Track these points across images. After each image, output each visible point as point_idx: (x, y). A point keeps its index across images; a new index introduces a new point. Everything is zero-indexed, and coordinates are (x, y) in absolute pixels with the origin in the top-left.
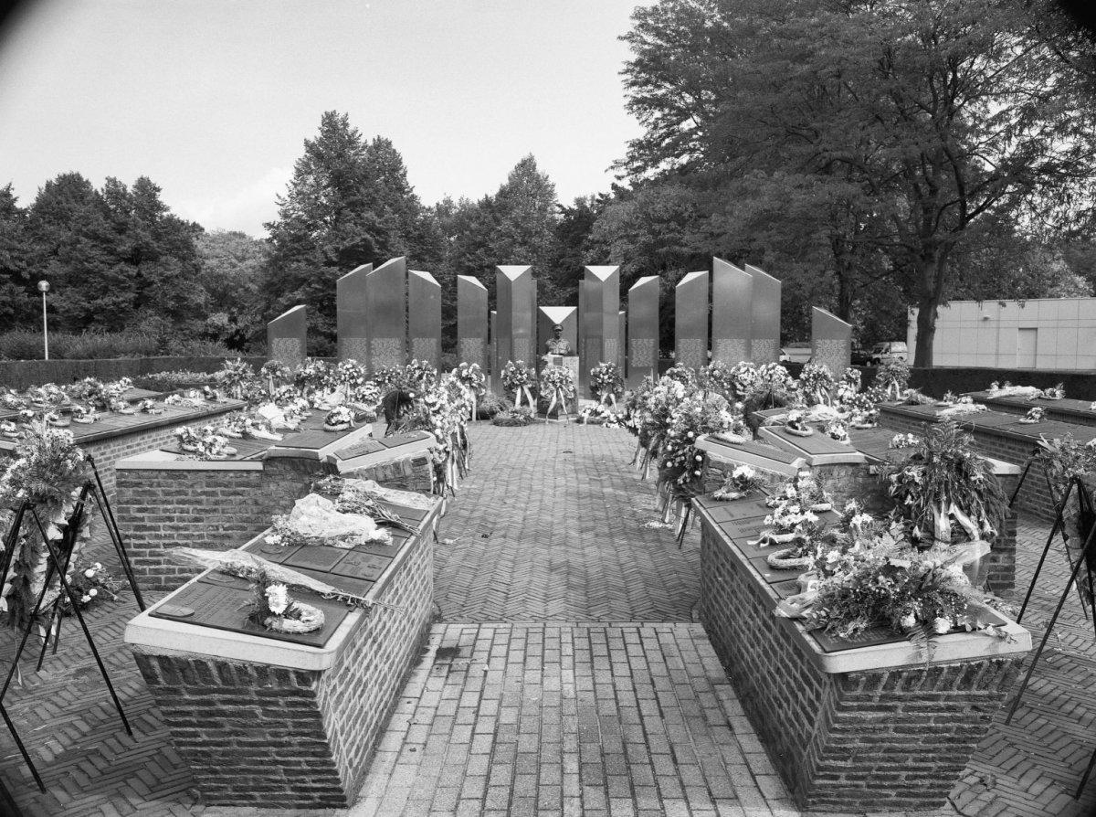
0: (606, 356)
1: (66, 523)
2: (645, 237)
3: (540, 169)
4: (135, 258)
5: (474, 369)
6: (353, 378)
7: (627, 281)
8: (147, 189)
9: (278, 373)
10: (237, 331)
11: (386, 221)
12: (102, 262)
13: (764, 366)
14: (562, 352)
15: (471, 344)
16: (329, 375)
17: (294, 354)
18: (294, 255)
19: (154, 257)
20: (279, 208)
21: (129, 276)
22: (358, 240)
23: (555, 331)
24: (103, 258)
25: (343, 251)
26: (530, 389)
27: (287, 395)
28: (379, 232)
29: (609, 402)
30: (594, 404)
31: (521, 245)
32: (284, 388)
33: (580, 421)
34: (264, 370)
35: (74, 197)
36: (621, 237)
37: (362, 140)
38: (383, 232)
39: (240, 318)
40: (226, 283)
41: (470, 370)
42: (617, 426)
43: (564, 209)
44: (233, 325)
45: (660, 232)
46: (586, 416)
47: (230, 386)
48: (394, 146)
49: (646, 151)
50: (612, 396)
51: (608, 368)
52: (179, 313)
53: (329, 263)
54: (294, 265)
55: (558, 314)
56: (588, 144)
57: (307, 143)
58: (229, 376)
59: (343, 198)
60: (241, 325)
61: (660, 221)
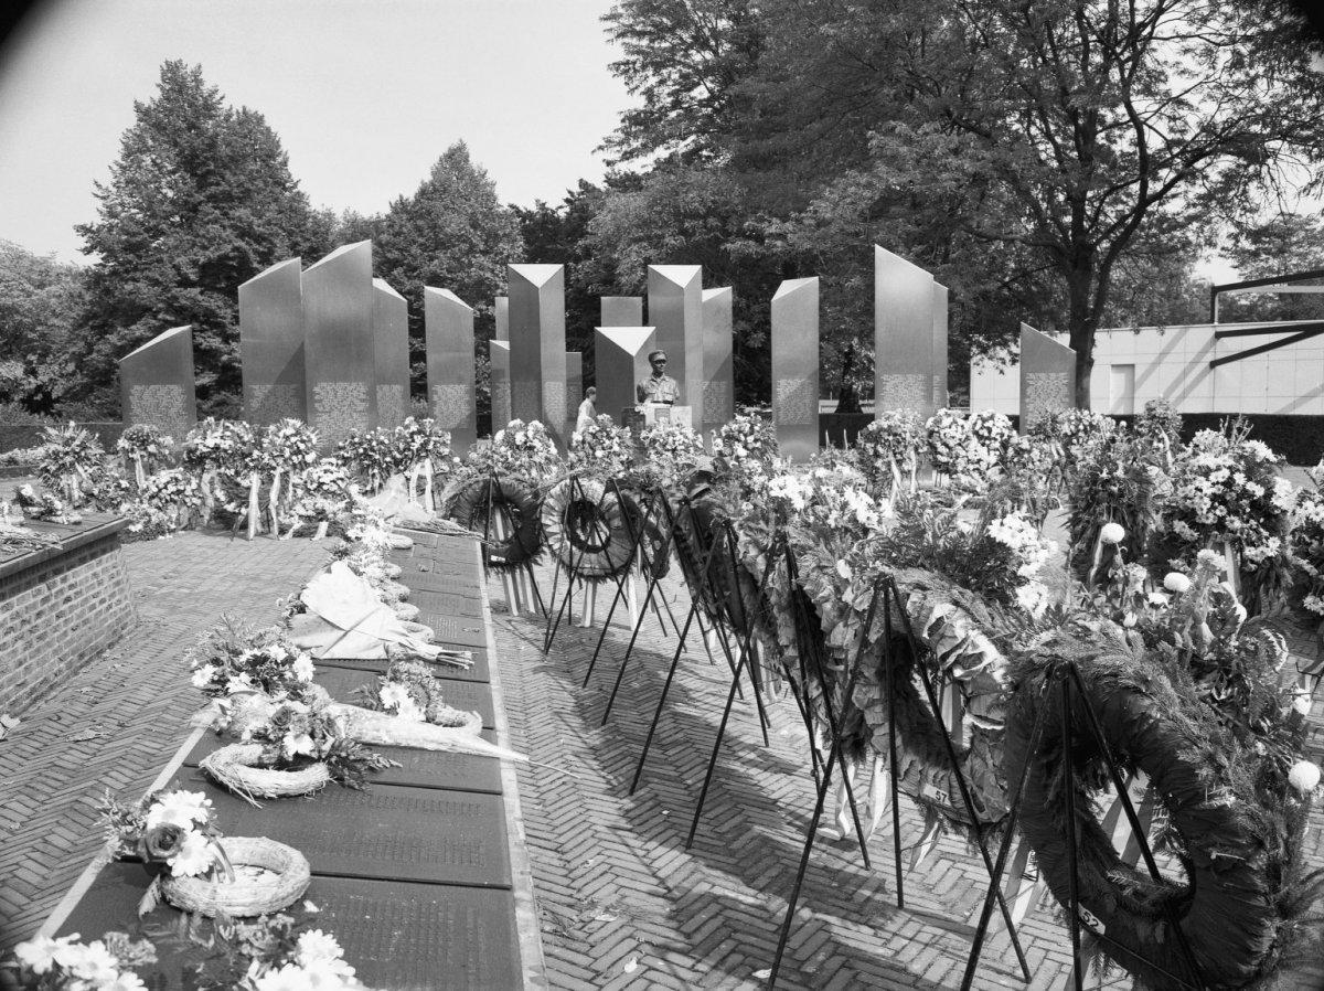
3: (475, 161)
5: (537, 431)
6: (298, 452)
9: (152, 448)
10: (39, 388)
11: (269, 223)
14: (669, 398)
16: (262, 449)
17: (173, 411)
18: (127, 271)
20: (99, 203)
22: (227, 248)
25: (204, 267)
27: (172, 488)
28: (259, 239)
31: (484, 253)
32: (164, 476)
34: (122, 443)
37: (225, 105)
38: (264, 239)
39: (41, 369)
40: (18, 318)
41: (530, 434)
44: (32, 379)
45: (694, 233)
47: (56, 475)
48: (268, 122)
49: (645, 126)
53: (185, 283)
54: (129, 287)
56: (559, 119)
57: (138, 107)
58: (56, 456)
59: (201, 187)
60: (43, 378)
61: (694, 215)
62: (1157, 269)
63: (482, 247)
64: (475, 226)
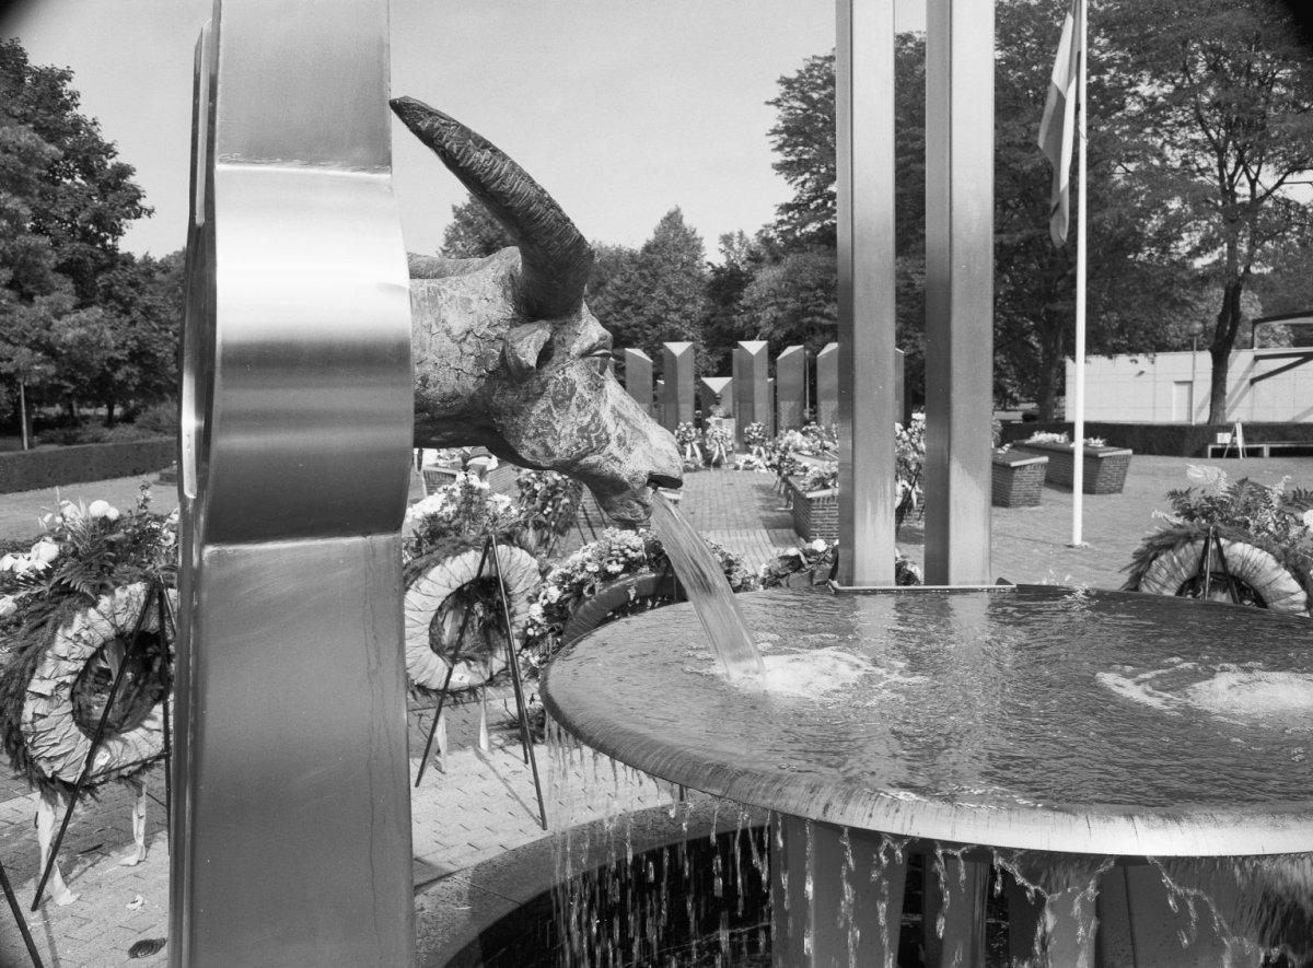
0: (757, 416)
1: (708, 420)
2: (792, 304)
3: (687, 222)
7: (774, 351)
15: (828, 407)
23: (715, 399)
29: (759, 454)
30: (748, 457)
36: (772, 305)
43: (713, 267)
46: (741, 464)
51: (758, 427)
55: (717, 384)
57: (454, 209)
61: (808, 288)
63: (675, 306)
64: (670, 293)
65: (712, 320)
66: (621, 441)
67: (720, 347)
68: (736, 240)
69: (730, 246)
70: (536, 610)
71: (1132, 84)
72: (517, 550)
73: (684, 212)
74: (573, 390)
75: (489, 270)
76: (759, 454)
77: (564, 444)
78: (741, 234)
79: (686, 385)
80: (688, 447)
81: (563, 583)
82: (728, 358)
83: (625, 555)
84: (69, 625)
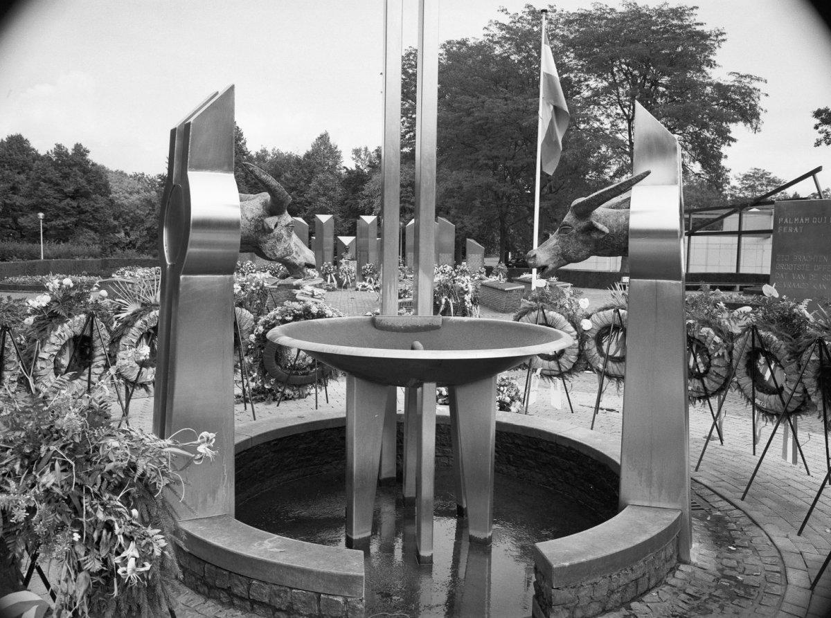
3: (332, 141)
4: (75, 195)
8: (80, 151)
12: (55, 198)
13: (442, 266)
19: (86, 195)
21: (73, 207)
23: (346, 249)
24: (55, 196)
26: (334, 275)
29: (370, 282)
30: (364, 283)
33: (357, 290)
35: (20, 151)
42: (373, 291)
44: (128, 238)
46: (360, 287)
50: (372, 279)
52: (104, 230)
55: (347, 240)
60: (133, 237)
62: (528, 212)
65: (346, 202)
66: (297, 253)
67: (348, 219)
68: (363, 153)
69: (359, 157)
70: (253, 337)
71: (586, 80)
72: (244, 310)
73: (330, 135)
74: (283, 237)
75: (257, 200)
76: (370, 282)
77: (279, 253)
78: (366, 149)
79: (329, 240)
80: (329, 277)
81: (266, 325)
82: (355, 225)
83: (294, 313)
84: (56, 330)
